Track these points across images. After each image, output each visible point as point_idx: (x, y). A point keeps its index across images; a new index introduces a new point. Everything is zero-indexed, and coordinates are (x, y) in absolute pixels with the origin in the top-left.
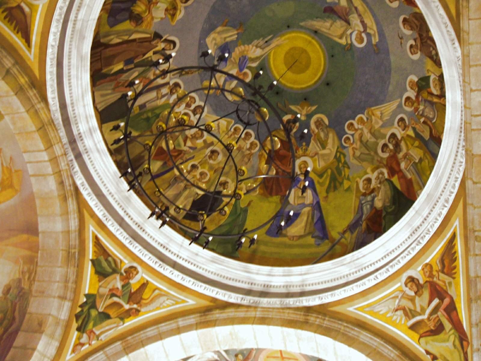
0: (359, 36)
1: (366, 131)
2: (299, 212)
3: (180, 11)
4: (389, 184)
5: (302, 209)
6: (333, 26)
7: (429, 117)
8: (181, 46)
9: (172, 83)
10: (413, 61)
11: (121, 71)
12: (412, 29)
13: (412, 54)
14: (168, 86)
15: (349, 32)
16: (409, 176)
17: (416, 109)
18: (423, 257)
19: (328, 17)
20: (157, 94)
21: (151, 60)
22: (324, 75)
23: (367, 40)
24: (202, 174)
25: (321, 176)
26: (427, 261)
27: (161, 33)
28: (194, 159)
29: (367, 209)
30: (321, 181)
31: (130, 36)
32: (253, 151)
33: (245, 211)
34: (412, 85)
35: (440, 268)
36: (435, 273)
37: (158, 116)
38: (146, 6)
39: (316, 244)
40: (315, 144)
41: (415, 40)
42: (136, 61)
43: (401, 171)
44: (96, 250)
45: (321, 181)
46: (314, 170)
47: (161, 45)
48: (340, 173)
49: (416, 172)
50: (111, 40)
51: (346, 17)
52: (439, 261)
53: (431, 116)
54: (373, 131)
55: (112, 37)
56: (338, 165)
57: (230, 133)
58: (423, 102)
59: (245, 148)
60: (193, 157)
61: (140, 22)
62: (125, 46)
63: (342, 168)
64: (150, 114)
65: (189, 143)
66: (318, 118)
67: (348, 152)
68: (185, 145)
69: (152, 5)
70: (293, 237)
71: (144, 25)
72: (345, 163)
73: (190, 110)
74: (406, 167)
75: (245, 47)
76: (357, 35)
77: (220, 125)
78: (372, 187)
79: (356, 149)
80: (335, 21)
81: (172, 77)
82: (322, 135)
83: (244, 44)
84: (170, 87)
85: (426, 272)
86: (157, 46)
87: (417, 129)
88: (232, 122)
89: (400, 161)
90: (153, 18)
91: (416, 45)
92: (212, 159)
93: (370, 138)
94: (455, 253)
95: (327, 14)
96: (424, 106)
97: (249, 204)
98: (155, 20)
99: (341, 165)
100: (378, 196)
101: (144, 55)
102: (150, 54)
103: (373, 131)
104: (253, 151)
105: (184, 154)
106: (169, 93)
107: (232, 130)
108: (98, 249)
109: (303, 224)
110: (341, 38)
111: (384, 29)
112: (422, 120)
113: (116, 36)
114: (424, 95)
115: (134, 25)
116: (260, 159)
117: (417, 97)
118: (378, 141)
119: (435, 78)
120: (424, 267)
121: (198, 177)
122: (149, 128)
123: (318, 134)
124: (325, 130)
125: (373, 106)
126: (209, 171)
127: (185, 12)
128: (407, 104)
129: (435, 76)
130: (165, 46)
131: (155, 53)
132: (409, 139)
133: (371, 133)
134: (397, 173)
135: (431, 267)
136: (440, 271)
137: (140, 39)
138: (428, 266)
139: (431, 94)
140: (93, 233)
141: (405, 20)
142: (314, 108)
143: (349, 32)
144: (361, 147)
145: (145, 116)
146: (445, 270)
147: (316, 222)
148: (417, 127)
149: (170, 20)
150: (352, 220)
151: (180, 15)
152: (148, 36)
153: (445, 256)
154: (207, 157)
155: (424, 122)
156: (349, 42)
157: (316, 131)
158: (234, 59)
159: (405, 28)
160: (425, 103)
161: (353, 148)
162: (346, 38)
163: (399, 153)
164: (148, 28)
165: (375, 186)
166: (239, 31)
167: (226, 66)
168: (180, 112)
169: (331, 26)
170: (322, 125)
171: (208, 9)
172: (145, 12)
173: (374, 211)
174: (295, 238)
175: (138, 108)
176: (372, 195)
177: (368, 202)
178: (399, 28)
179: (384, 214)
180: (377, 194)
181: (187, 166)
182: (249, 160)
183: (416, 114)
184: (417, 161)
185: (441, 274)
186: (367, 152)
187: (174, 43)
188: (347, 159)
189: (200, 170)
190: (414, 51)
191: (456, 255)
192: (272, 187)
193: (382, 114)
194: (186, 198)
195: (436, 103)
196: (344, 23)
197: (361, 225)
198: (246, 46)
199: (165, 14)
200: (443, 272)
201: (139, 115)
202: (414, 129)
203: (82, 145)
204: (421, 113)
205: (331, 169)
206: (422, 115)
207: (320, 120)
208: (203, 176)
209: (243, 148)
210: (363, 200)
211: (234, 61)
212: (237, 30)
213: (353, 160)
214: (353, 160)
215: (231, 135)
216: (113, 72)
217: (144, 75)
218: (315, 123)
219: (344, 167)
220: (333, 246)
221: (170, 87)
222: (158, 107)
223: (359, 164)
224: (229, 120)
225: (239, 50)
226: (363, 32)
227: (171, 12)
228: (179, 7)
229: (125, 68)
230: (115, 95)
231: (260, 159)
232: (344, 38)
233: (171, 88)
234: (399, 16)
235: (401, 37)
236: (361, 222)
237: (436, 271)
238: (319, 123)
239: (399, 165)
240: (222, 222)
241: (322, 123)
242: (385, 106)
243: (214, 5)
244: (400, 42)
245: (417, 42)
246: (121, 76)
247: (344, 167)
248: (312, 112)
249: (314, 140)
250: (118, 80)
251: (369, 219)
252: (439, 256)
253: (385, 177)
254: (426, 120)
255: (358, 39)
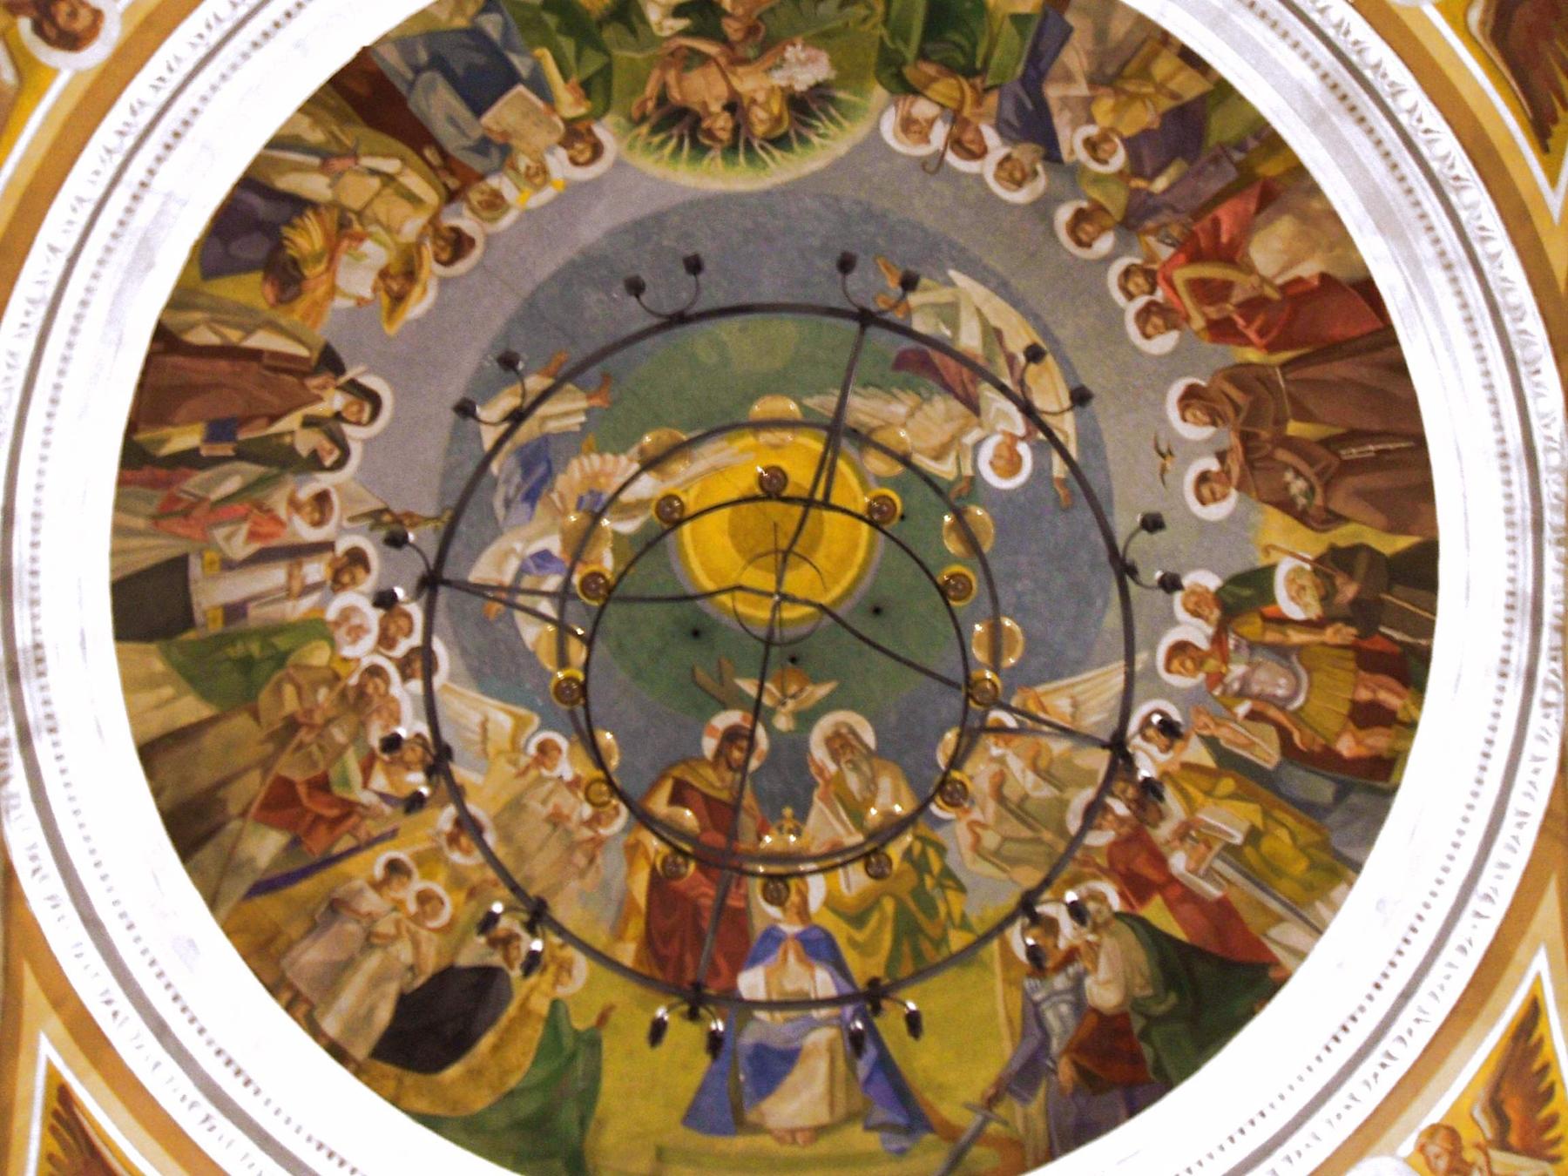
0: (1006, 453)
1: (1015, 765)
2: (796, 1044)
3: (425, 291)
4: (1133, 928)
5: (805, 1034)
6: (919, 415)
7: (1275, 696)
8: (395, 419)
9: (342, 546)
10: (1204, 526)
11: (190, 460)
12: (1214, 418)
13: (1203, 502)
14: (328, 556)
15: (969, 439)
16: (1213, 891)
17: (1216, 679)
18: (1417, 1105)
19: (905, 386)
20: (290, 576)
21: (292, 449)
22: (868, 580)
23: (1035, 463)
24: (424, 898)
25: (857, 919)
26: (1436, 1115)
27: (343, 352)
28: (396, 842)
29: (1061, 1018)
30: (860, 937)
31: (249, 332)
32: (603, 832)
33: (592, 1042)
34: (1196, 604)
35: (1489, 1134)
36: (1470, 1155)
37: (280, 659)
38: (327, 236)
39: (890, 1151)
40: (827, 811)
41: (1221, 456)
42: (243, 436)
43: (1172, 880)
44: (56, 1148)
45: (860, 937)
46: (831, 903)
47: (332, 400)
48: (929, 908)
49: (1247, 877)
50: (192, 326)
51: (971, 388)
52: (1484, 1111)
53: (1280, 692)
54: (1042, 763)
55: (198, 316)
56: (922, 880)
57: (524, 761)
58: (1245, 652)
59: (575, 818)
60: (393, 834)
61: (294, 289)
62: (223, 365)
63: (936, 893)
64: (255, 648)
65: (380, 781)
66: (838, 724)
67: (955, 837)
68: (365, 785)
69: (345, 243)
70: (793, 1132)
71: (301, 305)
72: (947, 873)
73: (390, 658)
74: (1192, 866)
75: (604, 462)
76: (998, 446)
77: (490, 726)
78: (1063, 944)
79: (984, 826)
80: (928, 400)
81: (346, 524)
82: (853, 782)
83: (601, 452)
84: (335, 559)
85: (1437, 1157)
86: (319, 399)
87: (1222, 742)
88: (531, 721)
89: (1165, 850)
90: (333, 291)
91: (1226, 473)
92: (460, 849)
93: (1036, 787)
94: (1545, 1068)
95: (903, 374)
96: (1249, 664)
97: (603, 1019)
98: (340, 303)
99: (929, 882)
100: (1096, 968)
101: (274, 419)
102: (291, 422)
103: (1042, 763)
104: (603, 832)
105: (363, 818)
106: (329, 583)
107: (532, 749)
108: (65, 1146)
109: (820, 1085)
110: (939, 456)
111: (1103, 425)
112: (1243, 709)
113: (207, 316)
114: (1245, 630)
115: (271, 298)
116: (631, 862)
117: (1218, 640)
118: (1067, 795)
119: (1298, 571)
120: (1424, 1140)
121: (412, 907)
122: (247, 702)
123: (840, 779)
124: (865, 768)
125: (1043, 681)
126: (448, 889)
127: (440, 298)
128: (1175, 664)
129: (1298, 562)
130: (347, 406)
131: (309, 423)
132: (1194, 776)
133: (1036, 769)
134: (1160, 888)
135: (1453, 1135)
136: (1490, 1143)
137: (275, 355)
138: (1442, 1133)
139: (1283, 621)
140: (52, 1073)
141: (1191, 397)
142: (823, 691)
143: (969, 439)
144: (999, 819)
145: (238, 650)
146: (1513, 1139)
147: (869, 1080)
148: (1224, 735)
149: (384, 313)
150: (1012, 1059)
151: (419, 306)
152: (303, 352)
153: (1505, 1086)
154: (443, 841)
155: (1253, 716)
156: (968, 471)
157: (832, 768)
158: (562, 497)
159: (1184, 419)
160: (1251, 654)
161: (972, 825)
162: (958, 458)
163: (1155, 826)
164: (309, 323)
165: (1078, 942)
166: (597, 402)
167: (530, 519)
168: (358, 660)
169: (911, 414)
170: (853, 748)
171: (511, 304)
172: (317, 258)
173: (1091, 1020)
174: (800, 1138)
175: (220, 613)
176: (1071, 970)
177: (1057, 993)
178: (1164, 420)
179: (1138, 1024)
180: (1090, 967)
181: (372, 865)
182: (592, 860)
183: (1217, 692)
184: (1238, 839)
185: (1497, 1156)
186: (1026, 833)
187: (374, 399)
188: (952, 861)
189: (418, 884)
190: (1213, 493)
191: (1551, 1077)
192: (681, 957)
193: (1075, 705)
194: (377, 981)
195: (1300, 648)
196: (958, 408)
197: (1054, 1072)
198: (609, 457)
199: (375, 290)
200: (1504, 1146)
201: (222, 640)
202: (1211, 743)
203: (39, 696)
204: (1236, 686)
205: (893, 895)
206: (1242, 695)
207: (844, 731)
208: (428, 908)
209: (568, 818)
210: (1036, 989)
211: (559, 504)
212: (589, 397)
213: (974, 862)
214: (974, 862)
215: (528, 768)
216: (167, 450)
217: (258, 495)
218: (829, 741)
219: (943, 887)
220: (956, 1159)
221: (335, 559)
222: (282, 628)
223: (1003, 876)
224: (522, 711)
225: (582, 469)
226: (1023, 439)
227: (395, 287)
228: (424, 274)
229: (204, 452)
230: (151, 542)
231: (631, 862)
232: (951, 459)
233: (339, 565)
234: (1169, 382)
235: (1164, 448)
236: (1050, 1064)
237: (1478, 1146)
238: (841, 743)
239: (1160, 860)
240: (513, 1081)
241: (854, 742)
242: (1085, 681)
243: (533, 294)
244: (1158, 470)
245: (1229, 461)
246: (187, 477)
247: (943, 887)
248: (819, 702)
249: (825, 798)
250: (174, 490)
251: (1077, 1049)
252: (1482, 1093)
253: (1110, 907)
254: (1260, 707)
255: (1001, 463)
